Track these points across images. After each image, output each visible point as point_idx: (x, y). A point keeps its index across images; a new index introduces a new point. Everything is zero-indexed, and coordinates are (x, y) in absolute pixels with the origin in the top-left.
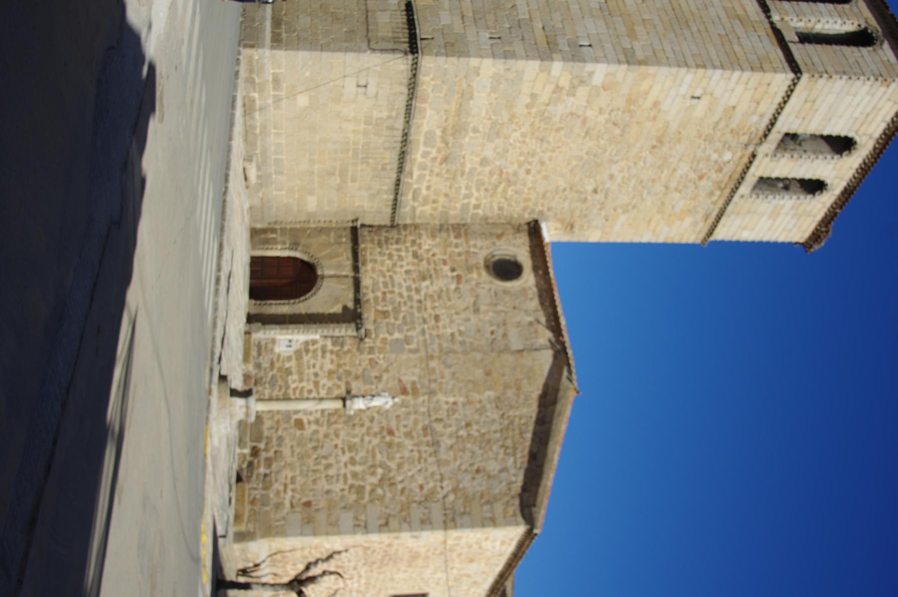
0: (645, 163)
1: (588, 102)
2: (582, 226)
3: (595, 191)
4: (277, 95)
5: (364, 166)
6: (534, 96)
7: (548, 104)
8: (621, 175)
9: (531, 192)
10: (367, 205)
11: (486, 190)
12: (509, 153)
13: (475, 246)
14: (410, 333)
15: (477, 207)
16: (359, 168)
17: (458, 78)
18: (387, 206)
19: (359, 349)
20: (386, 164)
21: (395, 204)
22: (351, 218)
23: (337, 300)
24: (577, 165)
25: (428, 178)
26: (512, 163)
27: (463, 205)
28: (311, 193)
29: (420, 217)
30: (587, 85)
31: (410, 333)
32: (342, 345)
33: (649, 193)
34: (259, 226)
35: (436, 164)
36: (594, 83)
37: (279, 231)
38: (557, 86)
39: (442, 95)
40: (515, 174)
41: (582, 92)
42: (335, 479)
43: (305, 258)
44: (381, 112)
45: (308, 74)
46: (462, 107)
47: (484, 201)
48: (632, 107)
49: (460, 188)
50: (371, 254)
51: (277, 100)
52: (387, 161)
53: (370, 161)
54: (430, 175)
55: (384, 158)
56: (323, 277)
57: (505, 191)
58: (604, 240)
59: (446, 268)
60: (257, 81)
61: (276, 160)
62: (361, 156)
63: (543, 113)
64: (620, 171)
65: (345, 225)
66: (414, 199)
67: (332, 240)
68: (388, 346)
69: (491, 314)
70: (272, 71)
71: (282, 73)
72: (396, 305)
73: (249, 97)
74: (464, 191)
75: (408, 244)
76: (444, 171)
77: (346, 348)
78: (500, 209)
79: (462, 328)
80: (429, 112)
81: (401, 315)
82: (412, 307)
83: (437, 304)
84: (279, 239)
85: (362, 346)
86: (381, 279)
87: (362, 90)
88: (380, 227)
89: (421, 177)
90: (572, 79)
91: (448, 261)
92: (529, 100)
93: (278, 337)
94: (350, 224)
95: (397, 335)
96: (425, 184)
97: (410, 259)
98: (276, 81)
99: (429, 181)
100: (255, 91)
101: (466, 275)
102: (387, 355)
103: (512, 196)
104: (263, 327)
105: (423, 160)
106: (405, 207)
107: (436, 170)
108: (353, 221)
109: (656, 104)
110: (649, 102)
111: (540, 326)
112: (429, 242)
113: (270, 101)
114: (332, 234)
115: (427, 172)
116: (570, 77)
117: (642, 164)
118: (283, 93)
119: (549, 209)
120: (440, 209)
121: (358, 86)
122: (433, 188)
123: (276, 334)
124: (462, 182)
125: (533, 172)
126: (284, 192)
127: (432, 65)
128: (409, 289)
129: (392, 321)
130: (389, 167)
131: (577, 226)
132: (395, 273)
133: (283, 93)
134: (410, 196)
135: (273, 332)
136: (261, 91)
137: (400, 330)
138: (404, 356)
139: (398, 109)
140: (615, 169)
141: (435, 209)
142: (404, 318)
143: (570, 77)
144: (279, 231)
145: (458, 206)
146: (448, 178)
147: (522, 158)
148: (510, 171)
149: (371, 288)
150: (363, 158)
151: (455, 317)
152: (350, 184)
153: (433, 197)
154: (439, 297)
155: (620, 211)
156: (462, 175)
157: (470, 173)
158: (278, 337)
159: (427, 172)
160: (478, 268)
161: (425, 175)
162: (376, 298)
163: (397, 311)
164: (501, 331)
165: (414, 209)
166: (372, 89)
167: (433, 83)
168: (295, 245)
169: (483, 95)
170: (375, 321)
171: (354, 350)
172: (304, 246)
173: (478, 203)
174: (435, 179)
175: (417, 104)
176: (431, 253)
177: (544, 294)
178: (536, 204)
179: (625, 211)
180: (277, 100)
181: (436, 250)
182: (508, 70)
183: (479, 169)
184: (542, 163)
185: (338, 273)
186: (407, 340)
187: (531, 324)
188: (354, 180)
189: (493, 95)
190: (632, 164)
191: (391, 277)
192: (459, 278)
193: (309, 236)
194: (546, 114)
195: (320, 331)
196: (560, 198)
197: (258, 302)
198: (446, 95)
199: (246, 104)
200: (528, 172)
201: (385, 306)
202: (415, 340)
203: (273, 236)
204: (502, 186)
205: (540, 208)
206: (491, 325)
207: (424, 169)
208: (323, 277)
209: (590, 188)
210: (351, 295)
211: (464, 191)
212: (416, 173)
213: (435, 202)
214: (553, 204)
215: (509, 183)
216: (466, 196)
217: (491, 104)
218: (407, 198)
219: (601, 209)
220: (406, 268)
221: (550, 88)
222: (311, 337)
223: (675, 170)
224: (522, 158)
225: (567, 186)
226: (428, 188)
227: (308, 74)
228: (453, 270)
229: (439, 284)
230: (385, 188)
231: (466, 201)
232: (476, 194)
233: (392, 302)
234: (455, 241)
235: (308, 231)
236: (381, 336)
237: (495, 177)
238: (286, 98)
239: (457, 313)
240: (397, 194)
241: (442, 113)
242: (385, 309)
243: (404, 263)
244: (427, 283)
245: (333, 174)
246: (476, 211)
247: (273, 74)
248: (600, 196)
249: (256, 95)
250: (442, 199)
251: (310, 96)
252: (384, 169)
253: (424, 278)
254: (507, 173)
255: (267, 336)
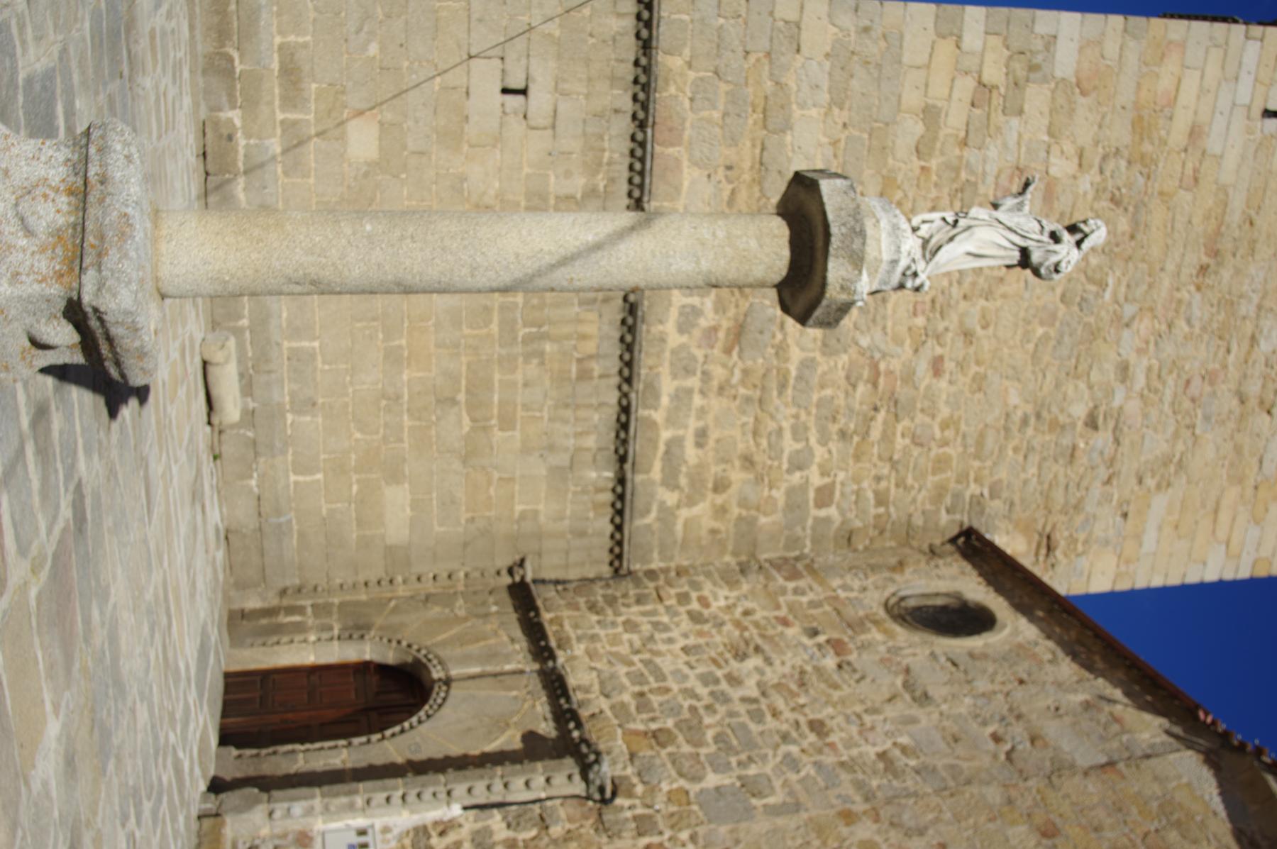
0: (1189, 321)
1: (1050, 133)
2: (1073, 540)
3: (1092, 423)
4: (295, 123)
5: (532, 369)
6: (930, 115)
7: (964, 143)
8: (1145, 362)
9: (949, 434)
10: (545, 509)
11: (843, 434)
12: (890, 306)
13: (845, 587)
14: (752, 770)
15: (825, 496)
16: (519, 377)
17: (752, 58)
18: (596, 506)
19: (601, 825)
20: (591, 357)
21: (621, 497)
22: (504, 562)
23: (502, 724)
24: (1046, 337)
25: (697, 401)
26: (899, 342)
27: (790, 492)
28: (395, 476)
29: (685, 545)
30: (1045, 80)
31: (752, 770)
32: (543, 823)
33: (1207, 418)
34: (253, 603)
35: (717, 352)
36: (1059, 74)
37: (309, 610)
38: (981, 83)
39: (716, 115)
40: (909, 377)
41: (1037, 98)
42: (857, 676)
43: (390, 657)
44: (568, 174)
45: (373, 49)
46: (765, 153)
47: (841, 476)
48: (1147, 147)
49: (780, 431)
50: (576, 626)
51: (295, 142)
52: (590, 347)
53: (548, 347)
54: (703, 393)
55: (583, 337)
56: (448, 682)
57: (887, 437)
58: (1124, 586)
59: (793, 632)
60: (239, 67)
61: (295, 355)
62: (522, 332)
63: (957, 171)
64: (1140, 351)
65: (493, 582)
66: (670, 482)
67: (461, 613)
68: (695, 808)
69: (968, 701)
70: (278, 40)
71: (305, 46)
72: (686, 715)
73: (217, 124)
74: (789, 445)
75: (672, 602)
76: (736, 378)
77: (556, 830)
78: (881, 500)
79: (904, 740)
80: (689, 176)
81: (710, 734)
82: (731, 714)
83: (802, 700)
84: (310, 621)
85: (608, 816)
86: (622, 670)
87: (514, 101)
88: (587, 582)
89: (682, 396)
90: (1010, 58)
91: (791, 618)
92: (920, 129)
93: (319, 825)
94: (507, 580)
95: (712, 780)
96: (693, 424)
97: (686, 624)
98: (291, 73)
99: (702, 412)
100: (233, 107)
101: (852, 638)
102: (701, 830)
103: (906, 451)
104: (265, 796)
105: (684, 339)
106: (647, 511)
107: (718, 372)
108: (510, 571)
109: (1195, 133)
110: (1178, 135)
111: (1119, 707)
112: (723, 592)
113: (275, 145)
114: (460, 602)
115: (694, 382)
116: (1006, 53)
117: (1181, 324)
118: (308, 117)
119: (994, 494)
120: (736, 511)
121: (505, 91)
122: (714, 435)
123: (309, 812)
124: (784, 413)
125: (949, 365)
126: (319, 476)
127: (686, 17)
128: (707, 679)
129: (686, 749)
130: (597, 368)
131: (1061, 538)
132: (658, 653)
133: (308, 117)
134: (656, 473)
135: (298, 808)
136: (250, 105)
137: (720, 767)
138: (761, 825)
139: (609, 164)
140: (1128, 342)
141: (721, 511)
142: (718, 738)
143: (1006, 53)
144: (309, 610)
145: (779, 495)
146: (748, 400)
147: (920, 321)
148: (896, 365)
149: (596, 687)
150: (528, 340)
151: (868, 719)
152: (498, 435)
153: (715, 469)
154: (802, 684)
155: (1150, 482)
156: (782, 386)
157: (799, 378)
158: (319, 825)
159: (694, 382)
160: (876, 623)
161: (689, 392)
162: (619, 709)
163: (692, 728)
164: (1018, 731)
165: (667, 515)
166: (540, 99)
167: (692, 75)
168: (356, 630)
169: (814, 112)
170: (632, 756)
171: (588, 828)
172: (381, 628)
173: (827, 480)
174: (717, 404)
175: (663, 152)
176: (739, 610)
177: (1078, 648)
178: (962, 478)
179: (1162, 486)
180: (295, 142)
181: (749, 605)
182: (866, 30)
183: (823, 364)
184: (968, 335)
185: (490, 668)
186: (751, 787)
187: (1087, 706)
188: (507, 422)
189: (839, 116)
190: (1164, 327)
191: (647, 663)
192: (838, 646)
193: (395, 610)
194: (964, 175)
195: (460, 789)
196: (1016, 450)
197: (249, 752)
198: (725, 115)
199: (209, 150)
200: (937, 367)
201: (653, 719)
202: (777, 784)
203: (297, 618)
204: (881, 416)
205: (974, 489)
206: (984, 723)
207: (689, 372)
208: (448, 682)
209: (1080, 411)
210: (542, 706)
211: (789, 445)
212: (667, 386)
213: (720, 486)
214: (1003, 474)
215: (897, 408)
216: (798, 464)
217: (835, 143)
218: (643, 522)
219: (1108, 481)
220: (682, 642)
221: (966, 86)
222: (432, 814)
223: (1253, 339)
224: (920, 321)
225: (1029, 409)
226: (701, 435)
227: (373, 49)
228: (814, 633)
229: (784, 665)
230: (590, 442)
231: (797, 477)
232: (820, 452)
233: (674, 710)
234: (791, 585)
235: (393, 603)
236: (665, 787)
237: (862, 388)
238: (318, 135)
239: (873, 711)
240: (622, 459)
241: (721, 172)
242: (654, 726)
243: (675, 634)
244: (754, 662)
245: (454, 402)
246: (823, 513)
247: (281, 48)
248: (1103, 439)
249: (235, 116)
250: (737, 476)
251: (381, 123)
252: (584, 375)
253: (741, 656)
254: (890, 373)
255: (280, 825)
